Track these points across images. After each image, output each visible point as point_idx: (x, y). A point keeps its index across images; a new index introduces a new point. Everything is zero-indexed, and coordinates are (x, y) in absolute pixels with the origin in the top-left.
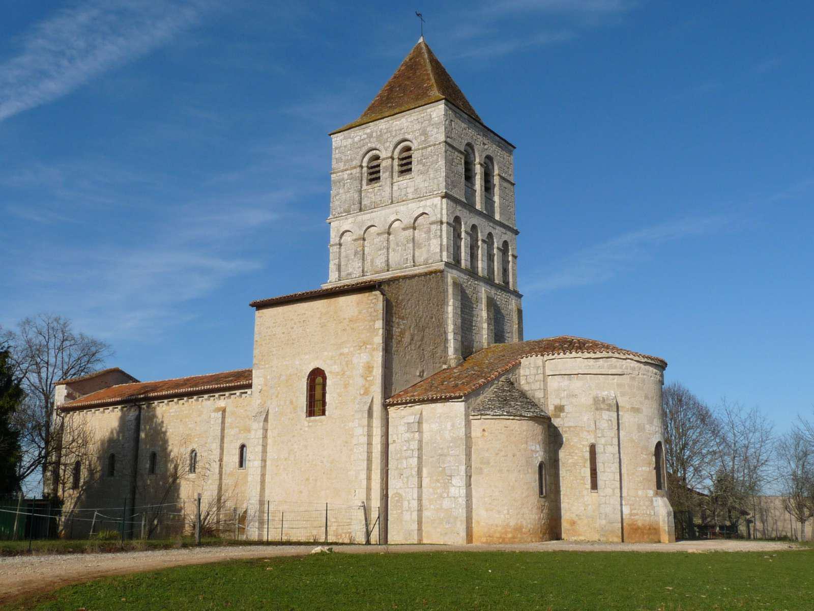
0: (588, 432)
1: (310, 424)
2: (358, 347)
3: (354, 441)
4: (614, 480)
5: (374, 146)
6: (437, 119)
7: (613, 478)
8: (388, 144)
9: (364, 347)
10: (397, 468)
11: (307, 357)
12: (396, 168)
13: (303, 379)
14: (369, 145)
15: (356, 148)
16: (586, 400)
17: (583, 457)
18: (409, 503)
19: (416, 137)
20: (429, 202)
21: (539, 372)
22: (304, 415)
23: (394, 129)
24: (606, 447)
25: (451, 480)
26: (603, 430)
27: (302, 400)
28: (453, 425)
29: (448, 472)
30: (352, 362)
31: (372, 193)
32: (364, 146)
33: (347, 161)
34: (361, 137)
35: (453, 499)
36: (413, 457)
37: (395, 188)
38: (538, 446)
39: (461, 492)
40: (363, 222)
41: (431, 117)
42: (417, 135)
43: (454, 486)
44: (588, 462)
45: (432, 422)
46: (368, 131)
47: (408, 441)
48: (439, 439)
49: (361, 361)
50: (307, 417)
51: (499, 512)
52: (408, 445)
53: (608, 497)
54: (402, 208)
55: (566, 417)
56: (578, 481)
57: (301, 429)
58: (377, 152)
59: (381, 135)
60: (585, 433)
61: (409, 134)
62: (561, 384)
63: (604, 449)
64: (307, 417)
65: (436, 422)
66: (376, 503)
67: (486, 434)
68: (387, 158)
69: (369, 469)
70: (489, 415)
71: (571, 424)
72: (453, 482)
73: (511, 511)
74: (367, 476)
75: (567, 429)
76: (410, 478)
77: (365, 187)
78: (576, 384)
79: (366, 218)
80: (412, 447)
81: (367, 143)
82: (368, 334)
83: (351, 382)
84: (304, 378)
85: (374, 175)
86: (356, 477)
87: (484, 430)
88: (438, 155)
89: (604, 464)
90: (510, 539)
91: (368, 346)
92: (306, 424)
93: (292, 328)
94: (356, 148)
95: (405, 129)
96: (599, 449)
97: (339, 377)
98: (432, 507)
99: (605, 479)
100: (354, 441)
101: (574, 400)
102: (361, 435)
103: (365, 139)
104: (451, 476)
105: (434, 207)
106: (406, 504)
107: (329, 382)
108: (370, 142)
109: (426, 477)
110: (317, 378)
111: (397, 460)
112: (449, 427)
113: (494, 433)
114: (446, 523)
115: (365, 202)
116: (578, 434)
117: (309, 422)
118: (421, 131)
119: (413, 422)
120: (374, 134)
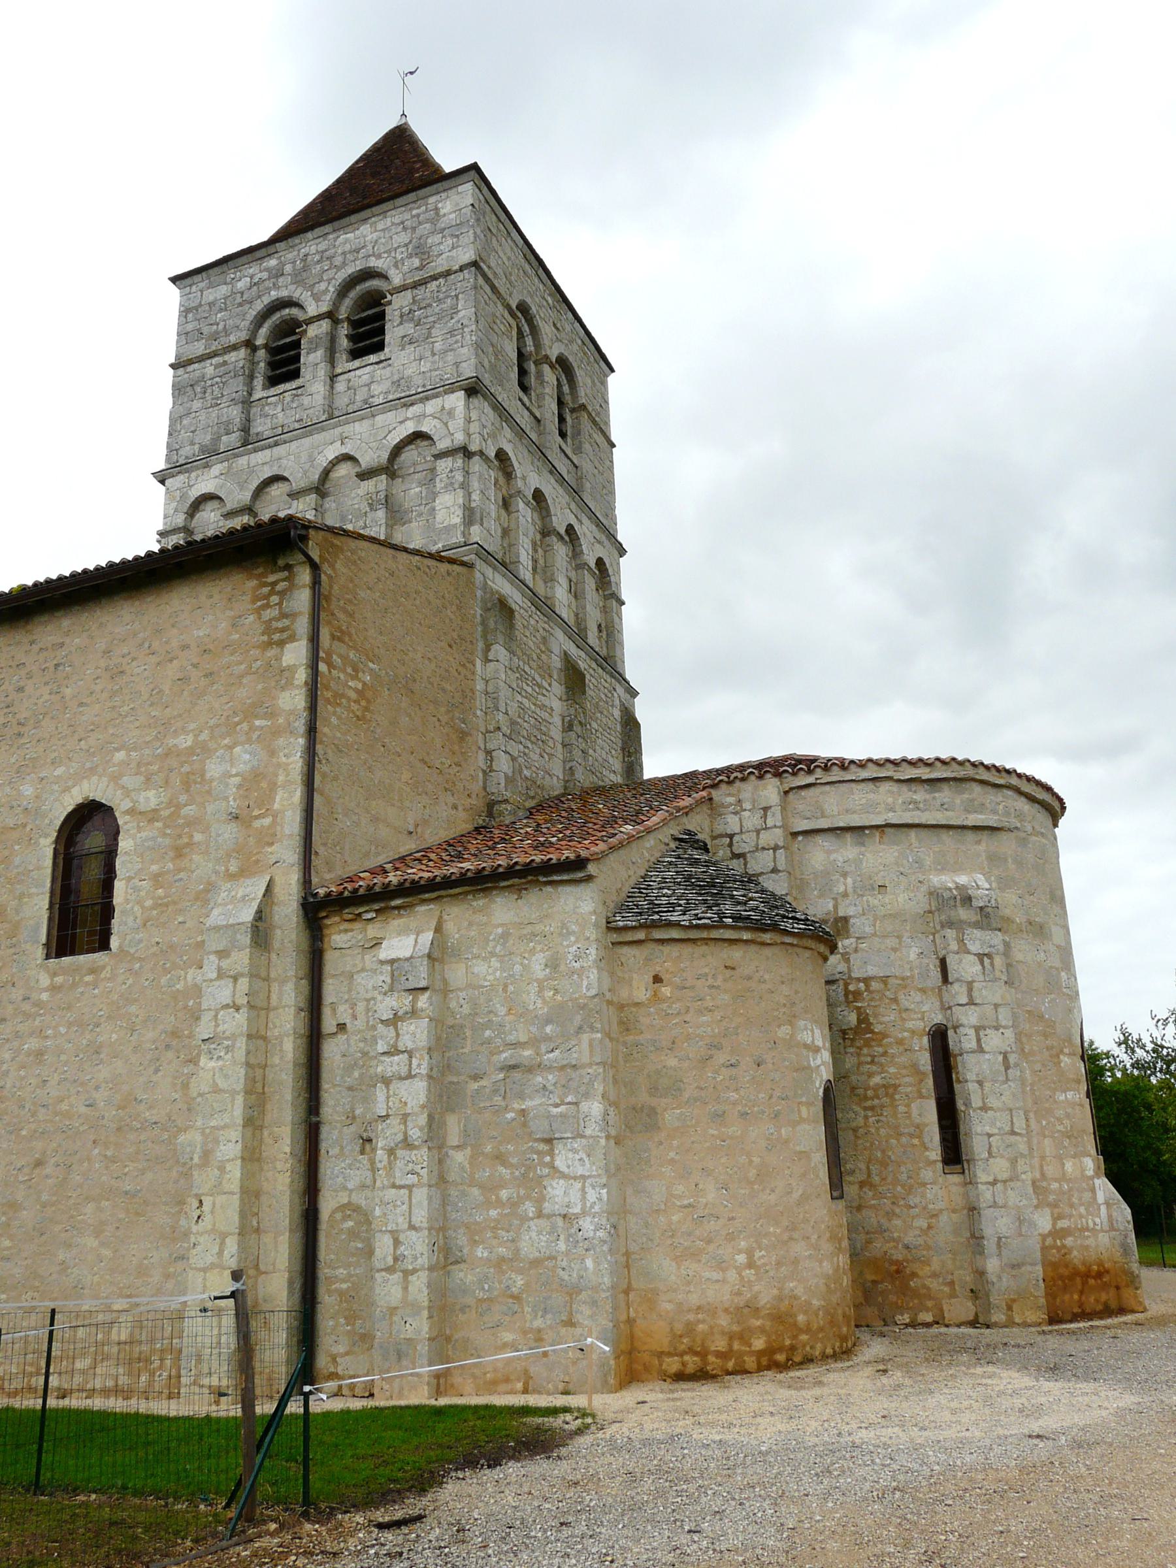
0: (923, 991)
1: (59, 980)
2: (224, 729)
3: (204, 1029)
4: (1013, 1133)
5: (284, 293)
6: (453, 216)
7: (1007, 1129)
8: (323, 286)
9: (245, 726)
10: (352, 1118)
11: (59, 771)
12: (344, 343)
13: (43, 841)
14: (273, 293)
15: (240, 305)
16: (905, 899)
17: (915, 1066)
18: (397, 1243)
19: (396, 262)
20: (432, 406)
21: (770, 823)
22: (40, 952)
23: (340, 251)
24: (982, 1033)
25: (551, 1153)
26: (970, 985)
27: (37, 908)
28: (553, 964)
29: (540, 1128)
30: (202, 776)
31: (278, 408)
32: (259, 297)
33: (215, 337)
34: (251, 278)
35: (560, 1222)
36: (410, 1076)
37: (340, 386)
38: (817, 1032)
39: (592, 1196)
40: (251, 470)
41: (437, 214)
42: (399, 257)
43: (564, 1176)
44: (930, 1082)
45: (477, 957)
46: (273, 262)
47: (395, 1020)
48: (502, 1011)
49: (234, 771)
50: (48, 957)
51: (721, 1265)
52: (392, 1033)
53: (999, 1186)
54: (360, 429)
55: (856, 951)
56: (904, 1140)
57: (26, 999)
58: (294, 311)
59: (305, 269)
60: (918, 996)
61: (379, 257)
62: (833, 856)
63: (979, 1040)
64: (48, 957)
65: (493, 954)
66: (277, 1289)
67: (666, 991)
68: (319, 317)
69: (253, 1122)
70: (670, 924)
71: (871, 971)
72: (558, 1163)
73: (758, 1254)
74: (245, 1148)
75: (862, 985)
76: (400, 1153)
77: (258, 394)
78: (879, 857)
79: (261, 463)
80: (406, 1042)
81: (269, 289)
82: (260, 687)
83: (198, 837)
84: (46, 836)
85: (283, 365)
86: (206, 1155)
87: (657, 979)
88: (457, 296)
89: (980, 1083)
90: (760, 1354)
91: (257, 723)
92: (45, 981)
93: (20, 689)
94: (240, 305)
95: (370, 247)
96: (962, 1041)
97: (159, 824)
98: (480, 1252)
99: (987, 1129)
100: (204, 1029)
101: (874, 901)
102: (227, 1006)
103: (262, 281)
104: (549, 1141)
105: (445, 418)
106: (383, 1246)
107: (124, 844)
108: (276, 287)
109: (458, 1147)
110: (85, 848)
111: (350, 1089)
112: (538, 968)
113: (693, 987)
114: (535, 1312)
115: (260, 426)
116: (895, 1000)
117: (55, 974)
118: (410, 246)
119: (411, 957)
120: (288, 268)
